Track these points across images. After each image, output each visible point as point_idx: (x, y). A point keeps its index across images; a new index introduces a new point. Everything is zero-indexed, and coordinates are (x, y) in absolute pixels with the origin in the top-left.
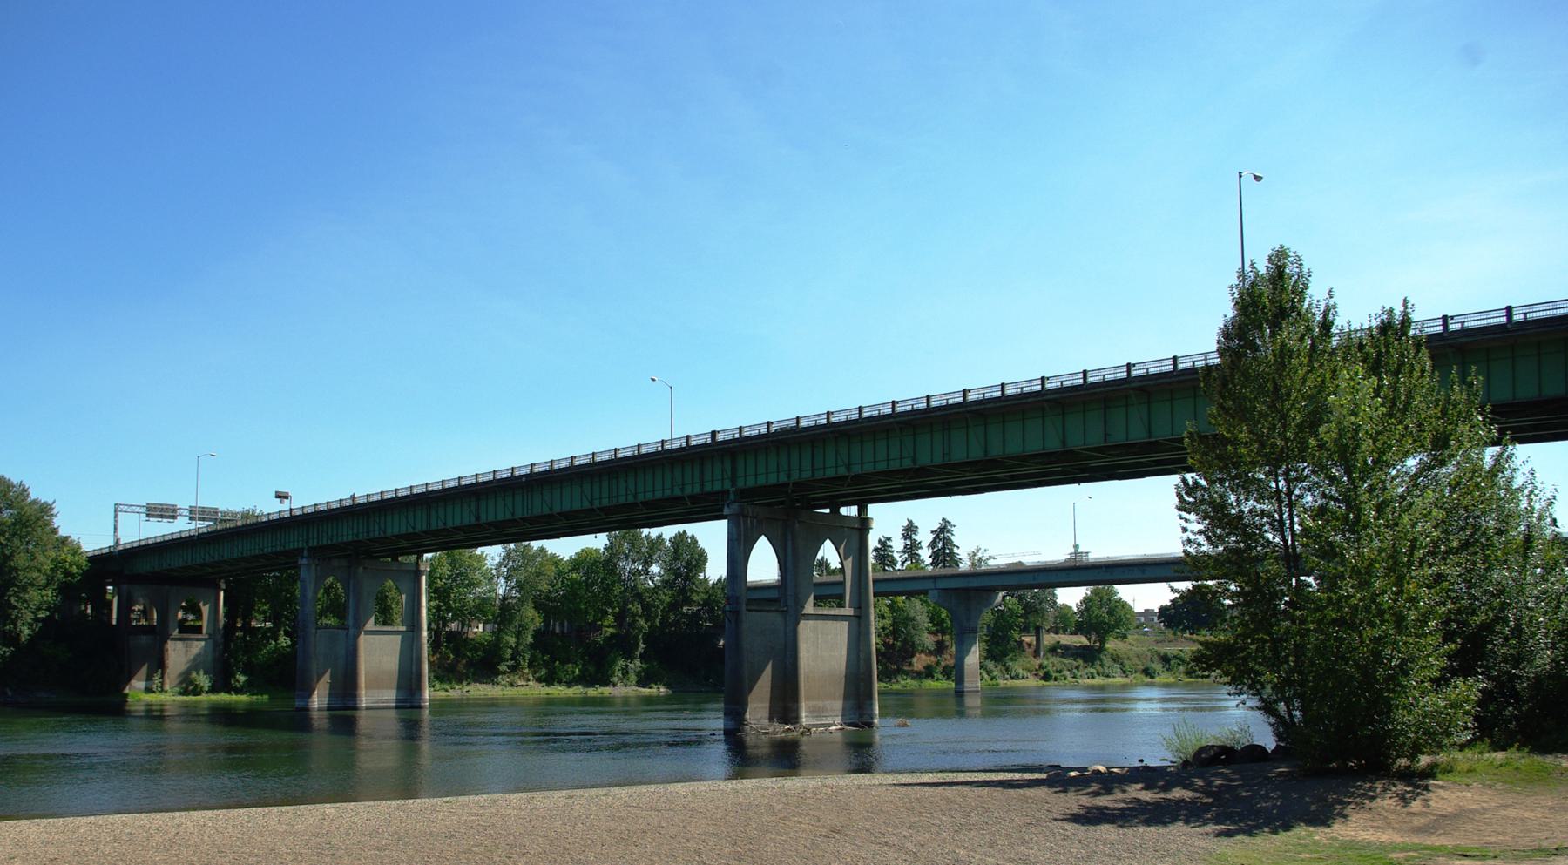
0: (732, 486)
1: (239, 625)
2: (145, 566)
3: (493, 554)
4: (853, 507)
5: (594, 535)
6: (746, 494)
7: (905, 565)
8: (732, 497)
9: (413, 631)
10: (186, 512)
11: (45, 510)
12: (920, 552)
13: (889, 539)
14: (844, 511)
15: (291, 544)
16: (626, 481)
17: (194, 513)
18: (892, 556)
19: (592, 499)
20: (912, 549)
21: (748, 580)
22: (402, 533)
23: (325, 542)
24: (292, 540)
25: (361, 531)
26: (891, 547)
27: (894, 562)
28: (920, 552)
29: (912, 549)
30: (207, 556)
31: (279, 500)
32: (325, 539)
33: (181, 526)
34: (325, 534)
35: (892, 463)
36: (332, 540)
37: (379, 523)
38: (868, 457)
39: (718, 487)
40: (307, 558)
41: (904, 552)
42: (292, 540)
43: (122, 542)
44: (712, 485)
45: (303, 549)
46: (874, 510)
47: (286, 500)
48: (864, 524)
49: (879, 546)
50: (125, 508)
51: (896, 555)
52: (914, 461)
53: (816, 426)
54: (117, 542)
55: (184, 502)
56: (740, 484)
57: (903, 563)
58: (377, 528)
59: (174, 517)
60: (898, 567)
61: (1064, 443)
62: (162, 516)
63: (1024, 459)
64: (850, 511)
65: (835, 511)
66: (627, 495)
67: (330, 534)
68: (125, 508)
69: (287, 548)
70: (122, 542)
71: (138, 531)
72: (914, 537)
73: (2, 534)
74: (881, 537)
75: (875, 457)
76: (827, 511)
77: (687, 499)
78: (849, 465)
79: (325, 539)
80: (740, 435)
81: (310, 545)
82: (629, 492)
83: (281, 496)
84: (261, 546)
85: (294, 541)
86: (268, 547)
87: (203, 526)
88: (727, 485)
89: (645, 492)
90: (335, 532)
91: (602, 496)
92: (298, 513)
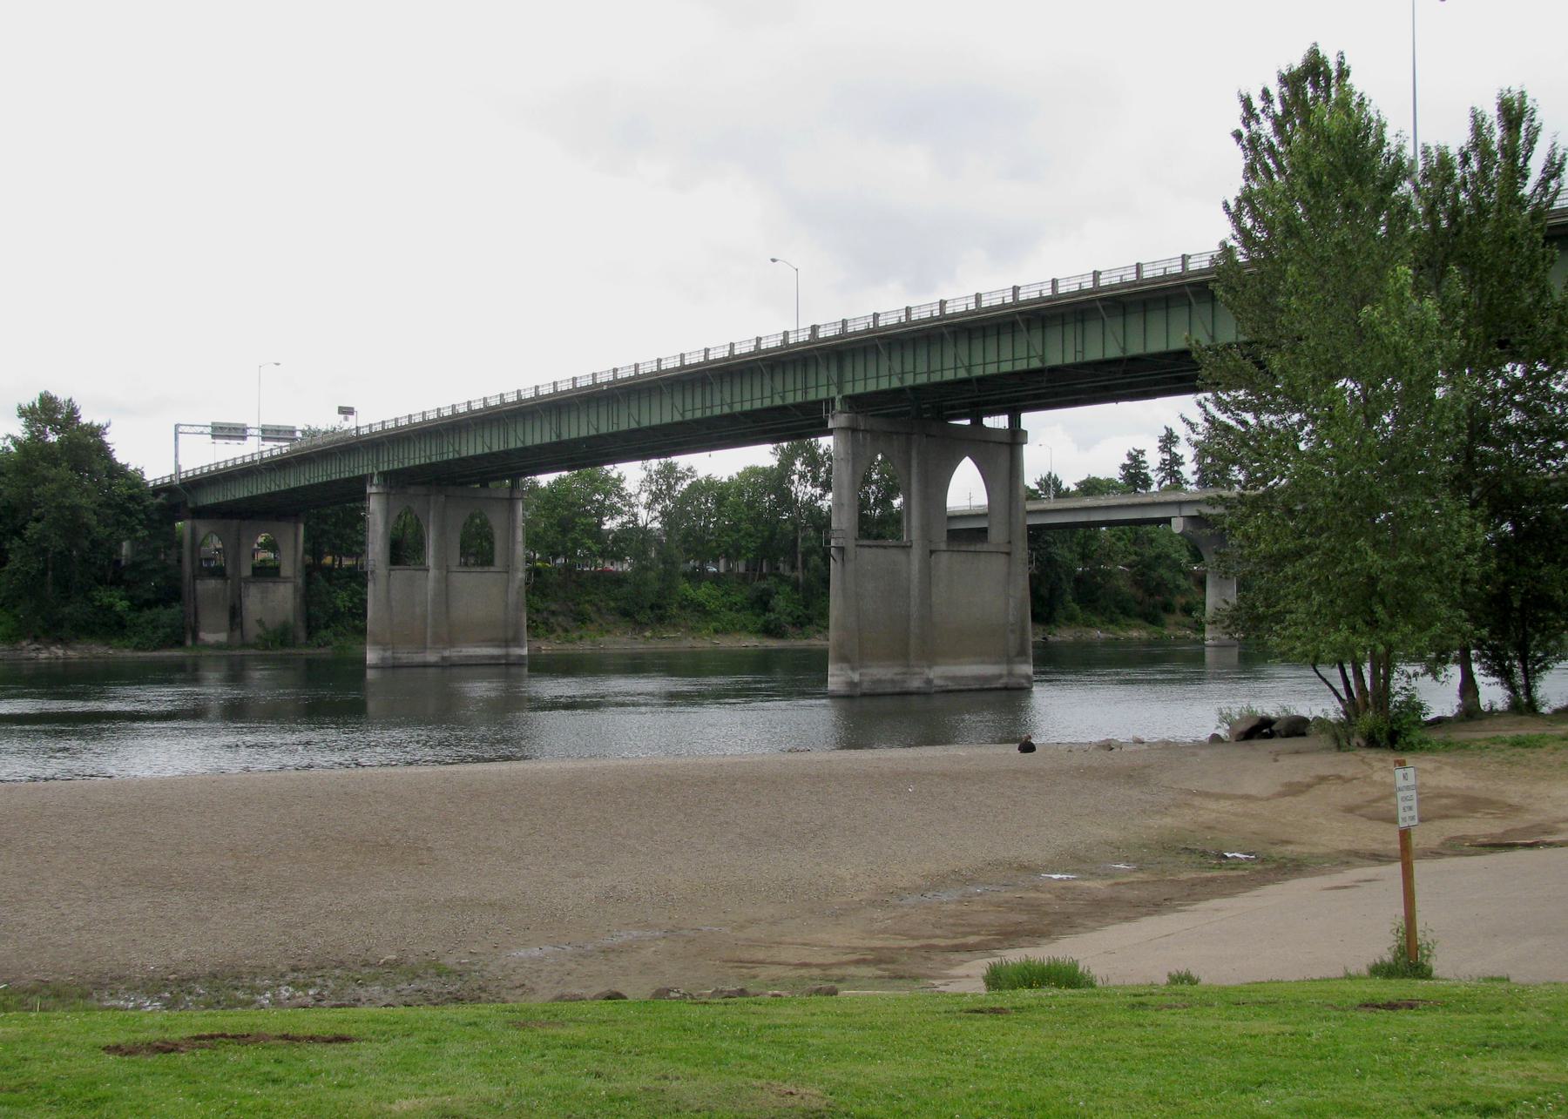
0: (838, 393)
1: (875, 477)
2: (210, 498)
3: (632, 474)
4: (1001, 417)
5: (708, 453)
6: (857, 403)
7: (1163, 485)
8: (838, 406)
9: (507, 572)
10: (256, 432)
11: (96, 432)
12: (1181, 469)
13: (1142, 452)
14: (989, 422)
15: (386, 464)
16: (721, 392)
17: (268, 433)
18: (1146, 474)
19: (684, 411)
20: (1171, 466)
21: (948, 506)
22: (572, 437)
23: (396, 467)
24: (412, 456)
25: (434, 453)
26: (1145, 462)
27: (1146, 482)
28: (1181, 469)
29: (1171, 466)
30: (273, 484)
31: (342, 416)
32: (396, 463)
33: (250, 449)
34: (422, 453)
35: (715, 409)
36: (430, 459)
37: (453, 446)
38: (978, 359)
39: (822, 394)
40: (377, 486)
41: (1161, 469)
42: (412, 456)
43: (183, 470)
44: (854, 385)
45: (372, 475)
46: (1028, 420)
47: (350, 417)
48: (1015, 438)
49: (1128, 462)
50: (187, 429)
51: (1152, 475)
52: (1042, 359)
53: (1165, 275)
54: (178, 467)
55: (251, 419)
56: (848, 390)
57: (1160, 484)
58: (451, 449)
59: (244, 438)
60: (1154, 488)
61: (1124, 349)
62: (229, 437)
63: (732, 417)
64: (998, 422)
65: (977, 422)
66: (722, 405)
67: (401, 457)
68: (187, 429)
69: (464, 454)
70: (183, 470)
71: (204, 455)
72: (1173, 449)
73: (2, 474)
74: (1132, 451)
75: (877, 373)
76: (967, 422)
77: (909, 391)
78: (970, 366)
79: (396, 463)
80: (1183, 269)
81: (381, 470)
82: (831, 382)
83: (346, 411)
84: (428, 453)
85: (394, 460)
86: (336, 473)
87: (271, 449)
88: (834, 392)
89: (693, 410)
90: (406, 455)
91: (755, 397)
92: (365, 431)
